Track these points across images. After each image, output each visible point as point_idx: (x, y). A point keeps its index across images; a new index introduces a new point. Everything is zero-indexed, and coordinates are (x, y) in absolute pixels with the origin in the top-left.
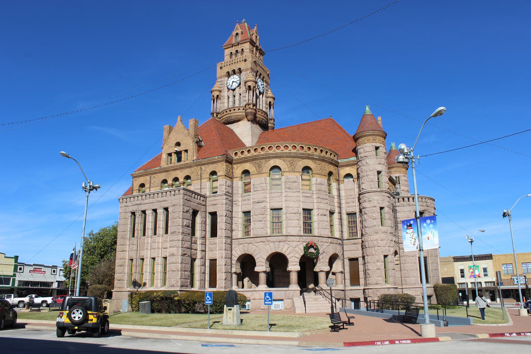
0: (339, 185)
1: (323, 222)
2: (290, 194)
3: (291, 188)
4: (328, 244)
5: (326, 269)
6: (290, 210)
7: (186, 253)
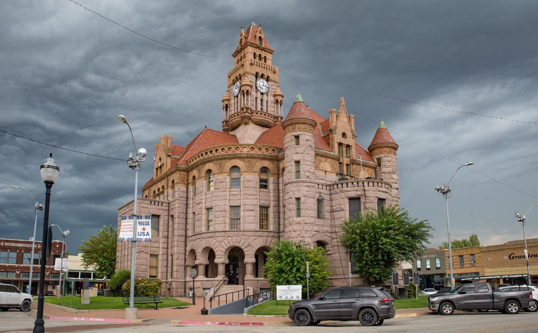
0: (278, 178)
2: (218, 194)
3: (219, 188)
5: (250, 261)
6: (248, 207)
7: (143, 250)
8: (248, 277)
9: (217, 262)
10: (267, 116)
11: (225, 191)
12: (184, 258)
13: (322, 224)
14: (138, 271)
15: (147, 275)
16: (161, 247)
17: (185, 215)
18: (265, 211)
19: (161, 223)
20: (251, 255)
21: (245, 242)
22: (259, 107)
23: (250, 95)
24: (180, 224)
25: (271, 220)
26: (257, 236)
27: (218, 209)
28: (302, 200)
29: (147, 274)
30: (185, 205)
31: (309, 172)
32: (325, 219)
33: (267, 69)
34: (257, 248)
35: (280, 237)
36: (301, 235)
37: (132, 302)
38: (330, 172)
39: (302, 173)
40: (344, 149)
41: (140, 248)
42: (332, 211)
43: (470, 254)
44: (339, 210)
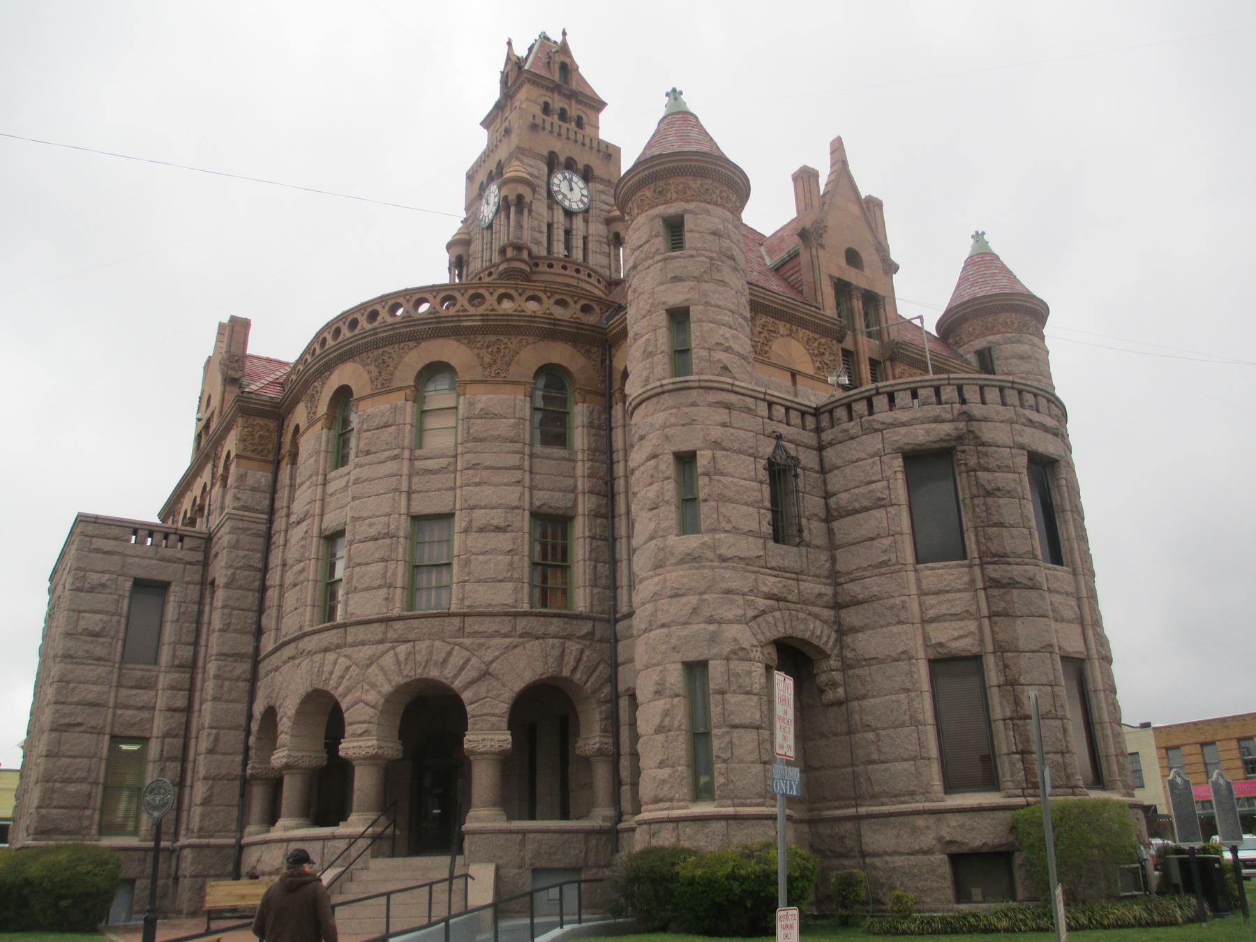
0: (609, 408)
1: (487, 557)
4: (508, 640)
5: (489, 743)
6: (480, 517)
7: (79, 720)
8: (478, 819)
9: (351, 752)
10: (583, 276)
11: (395, 458)
12: (240, 747)
13: (796, 566)
14: (48, 806)
15: (86, 823)
16: (161, 702)
17: (259, 575)
18: (554, 537)
19: (171, 611)
20: (494, 719)
21: (468, 660)
22: (559, 249)
23: (530, 211)
24: (234, 608)
25: (581, 571)
26: (521, 636)
27: (364, 530)
28: (703, 460)
29: (91, 818)
30: (261, 539)
31: (728, 350)
32: (808, 545)
33: (583, 144)
34: (519, 686)
35: (617, 641)
36: (706, 612)
37: (1048, 827)
38: (812, 377)
39: (698, 354)
40: (858, 305)
41: (67, 709)
42: (829, 517)
43: (1238, 735)
44: (866, 503)
